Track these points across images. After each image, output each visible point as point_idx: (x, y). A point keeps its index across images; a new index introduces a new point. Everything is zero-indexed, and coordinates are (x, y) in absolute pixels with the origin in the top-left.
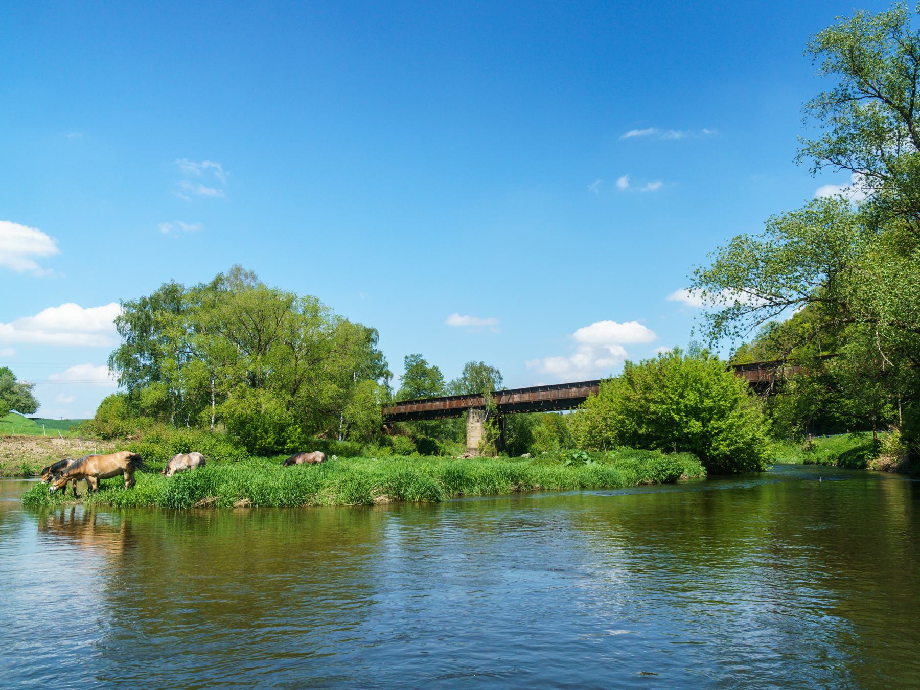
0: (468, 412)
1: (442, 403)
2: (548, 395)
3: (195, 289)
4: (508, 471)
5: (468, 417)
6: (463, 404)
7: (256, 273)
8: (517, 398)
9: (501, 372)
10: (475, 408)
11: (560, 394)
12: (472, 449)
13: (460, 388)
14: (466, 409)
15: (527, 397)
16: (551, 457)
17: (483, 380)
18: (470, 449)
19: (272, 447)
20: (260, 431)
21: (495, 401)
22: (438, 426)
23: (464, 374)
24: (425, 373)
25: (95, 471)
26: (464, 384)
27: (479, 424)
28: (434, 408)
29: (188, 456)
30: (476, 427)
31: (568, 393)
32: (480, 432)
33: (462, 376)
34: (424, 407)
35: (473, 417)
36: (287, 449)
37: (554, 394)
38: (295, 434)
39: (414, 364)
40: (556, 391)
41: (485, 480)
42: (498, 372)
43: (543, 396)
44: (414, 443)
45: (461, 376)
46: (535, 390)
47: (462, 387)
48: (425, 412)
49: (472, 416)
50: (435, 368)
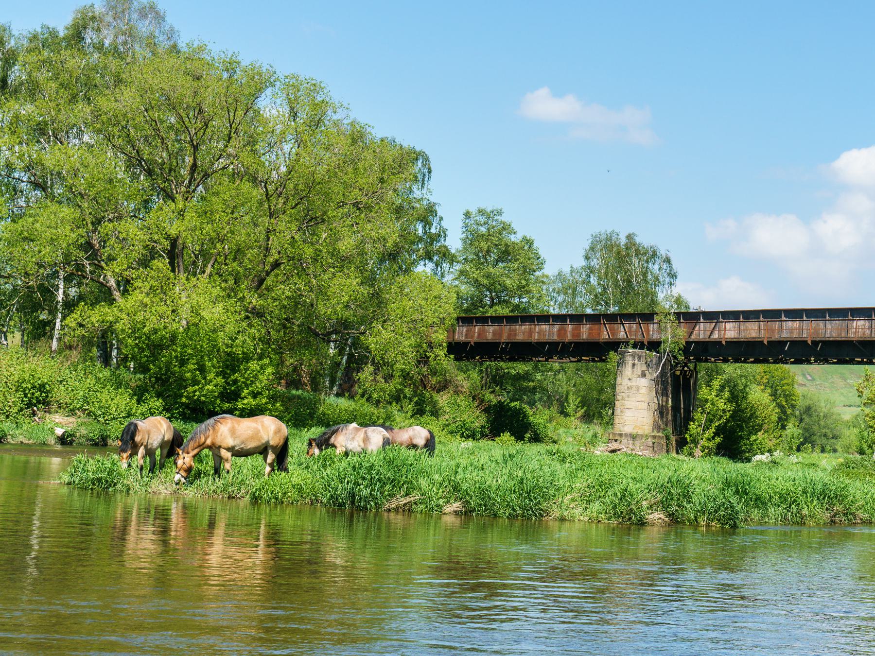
0: (623, 354)
1: (556, 328)
2: (801, 330)
3: (35, 37)
4: (819, 487)
5: (621, 363)
6: (605, 336)
7: (161, 7)
8: (730, 331)
9: (673, 261)
11: (831, 330)
12: (626, 435)
13: (575, 290)
14: (614, 345)
15: (753, 331)
16: (866, 468)
17: (631, 276)
18: (621, 435)
19: (213, 403)
20: (191, 367)
21: (682, 331)
22: (526, 377)
23: (587, 258)
24: (506, 254)
25: (230, 442)
26: (586, 282)
28: (536, 338)
29: (366, 432)
31: (848, 329)
32: (646, 398)
33: (583, 263)
34: (513, 333)
35: (634, 365)
37: (816, 330)
38: (260, 377)
39: (483, 230)
40: (821, 324)
41: (785, 500)
42: (668, 261)
43: (790, 330)
45: (581, 263)
46: (772, 315)
47: (580, 288)
49: (631, 362)
50: (529, 242)
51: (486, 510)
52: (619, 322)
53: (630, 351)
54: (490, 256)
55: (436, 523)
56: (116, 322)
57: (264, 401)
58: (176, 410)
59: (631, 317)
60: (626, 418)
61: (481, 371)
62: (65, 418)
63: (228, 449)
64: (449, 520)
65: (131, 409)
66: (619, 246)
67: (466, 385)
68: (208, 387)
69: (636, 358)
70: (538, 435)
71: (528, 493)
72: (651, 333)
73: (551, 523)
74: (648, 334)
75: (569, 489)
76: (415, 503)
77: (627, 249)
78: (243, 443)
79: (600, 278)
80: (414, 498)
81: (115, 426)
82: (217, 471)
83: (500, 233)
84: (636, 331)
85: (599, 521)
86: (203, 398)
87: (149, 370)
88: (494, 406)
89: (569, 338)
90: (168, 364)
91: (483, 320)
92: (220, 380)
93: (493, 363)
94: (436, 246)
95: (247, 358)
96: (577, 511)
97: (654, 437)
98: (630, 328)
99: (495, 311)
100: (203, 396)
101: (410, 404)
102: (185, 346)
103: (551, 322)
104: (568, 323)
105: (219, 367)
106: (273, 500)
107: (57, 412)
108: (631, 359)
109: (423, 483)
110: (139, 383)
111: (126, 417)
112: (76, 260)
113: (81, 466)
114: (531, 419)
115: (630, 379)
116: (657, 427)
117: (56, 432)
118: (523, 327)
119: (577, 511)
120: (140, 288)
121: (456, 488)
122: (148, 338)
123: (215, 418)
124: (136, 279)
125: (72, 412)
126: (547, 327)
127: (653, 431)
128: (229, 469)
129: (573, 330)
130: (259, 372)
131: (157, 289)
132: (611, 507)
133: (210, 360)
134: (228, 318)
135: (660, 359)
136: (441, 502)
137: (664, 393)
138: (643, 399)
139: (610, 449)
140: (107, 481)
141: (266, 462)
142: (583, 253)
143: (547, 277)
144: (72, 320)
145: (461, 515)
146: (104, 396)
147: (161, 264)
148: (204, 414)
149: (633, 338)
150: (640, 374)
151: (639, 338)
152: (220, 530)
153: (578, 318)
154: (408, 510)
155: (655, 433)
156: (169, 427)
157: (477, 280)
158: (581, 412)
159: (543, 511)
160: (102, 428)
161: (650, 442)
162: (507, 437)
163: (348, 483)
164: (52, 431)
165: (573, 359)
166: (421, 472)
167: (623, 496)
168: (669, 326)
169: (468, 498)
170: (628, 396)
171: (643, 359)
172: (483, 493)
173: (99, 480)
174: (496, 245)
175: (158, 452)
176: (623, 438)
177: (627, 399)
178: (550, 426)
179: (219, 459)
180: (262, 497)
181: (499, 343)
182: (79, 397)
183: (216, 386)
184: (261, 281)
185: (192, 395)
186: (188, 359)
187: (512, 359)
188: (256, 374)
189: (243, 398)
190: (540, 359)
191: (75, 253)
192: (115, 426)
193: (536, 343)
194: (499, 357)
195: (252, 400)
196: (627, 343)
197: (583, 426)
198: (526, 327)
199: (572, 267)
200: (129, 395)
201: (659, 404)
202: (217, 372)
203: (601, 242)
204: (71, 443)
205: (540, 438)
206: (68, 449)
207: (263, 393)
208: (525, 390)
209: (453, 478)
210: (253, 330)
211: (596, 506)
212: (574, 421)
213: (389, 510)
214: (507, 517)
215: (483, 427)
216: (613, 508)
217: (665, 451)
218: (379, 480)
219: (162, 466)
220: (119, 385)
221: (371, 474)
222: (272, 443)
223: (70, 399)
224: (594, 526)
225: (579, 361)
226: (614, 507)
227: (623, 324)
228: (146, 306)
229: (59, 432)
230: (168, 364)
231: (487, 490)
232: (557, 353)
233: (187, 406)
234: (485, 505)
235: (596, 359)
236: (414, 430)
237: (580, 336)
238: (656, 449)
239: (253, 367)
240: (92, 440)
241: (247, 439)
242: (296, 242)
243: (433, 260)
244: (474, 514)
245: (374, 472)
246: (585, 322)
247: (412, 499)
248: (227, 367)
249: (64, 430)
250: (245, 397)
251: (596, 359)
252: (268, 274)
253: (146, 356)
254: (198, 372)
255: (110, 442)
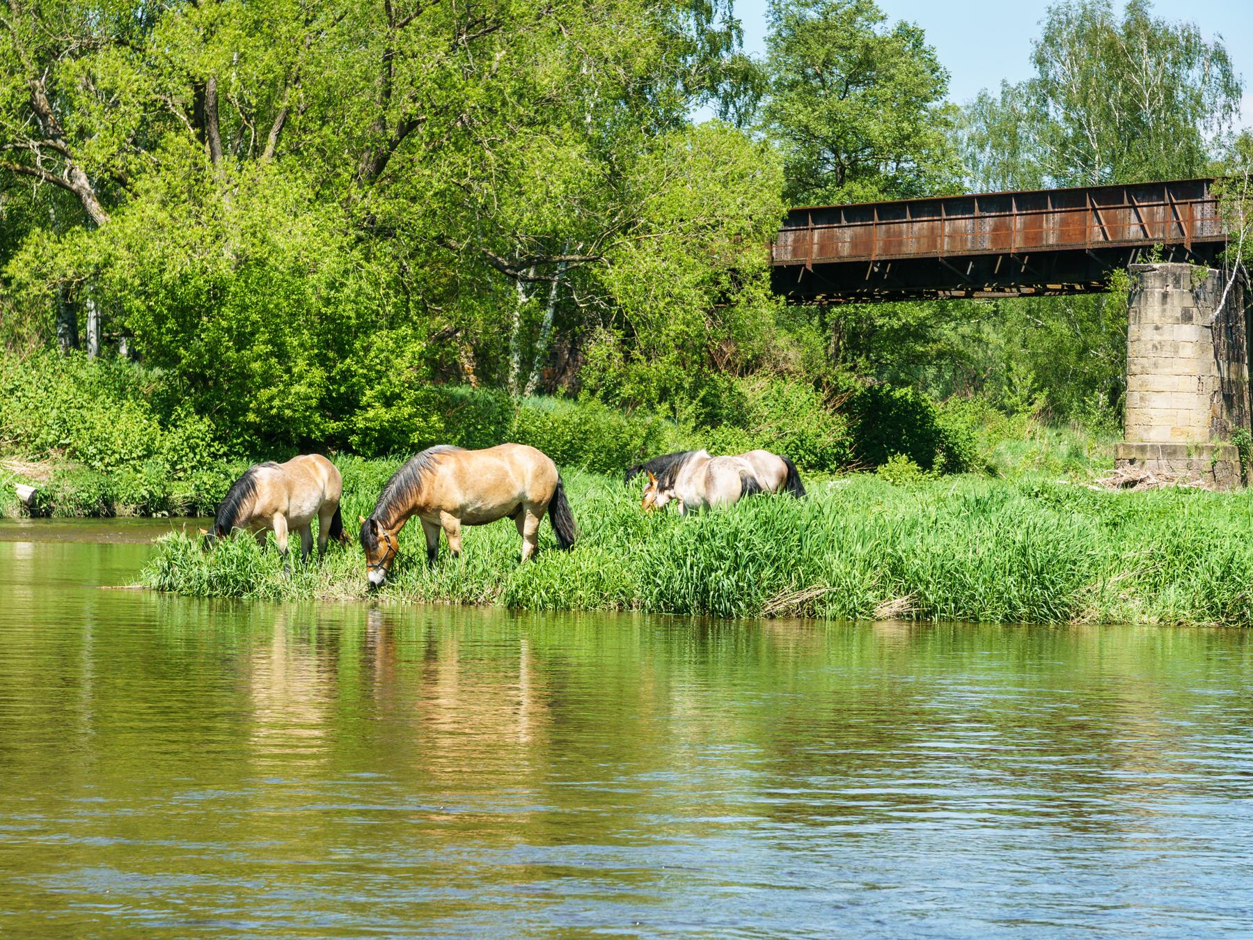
0: (1140, 274)
1: (988, 224)
5: (1136, 294)
10: (1175, 252)
13: (1014, 137)
14: (1118, 255)
18: (1142, 449)
19: (307, 421)
22: (918, 332)
23: (1041, 61)
25: (457, 498)
27: (1189, 332)
28: (945, 248)
30: (1176, 348)
32: (1195, 368)
33: (1034, 73)
34: (894, 241)
35: (1165, 296)
36: (366, 432)
38: (397, 362)
42: (1220, 57)
44: (840, 411)
48: (894, 262)
49: (1158, 292)
51: (957, 609)
52: (1126, 203)
53: (1156, 266)
54: (831, 73)
55: (862, 639)
56: (107, 264)
57: (407, 411)
58: (238, 438)
59: (1152, 191)
60: (1152, 412)
61: (824, 325)
62: (31, 464)
63: (454, 512)
64: (889, 630)
65: (153, 440)
66: (1109, 31)
67: (795, 357)
68: (296, 388)
69: (1170, 280)
70: (957, 456)
71: (1039, 574)
72: (1199, 223)
73: (1086, 630)
74: (1192, 227)
75: (1115, 564)
76: (821, 602)
77: (1129, 35)
78: (479, 498)
79: (1069, 106)
80: (818, 592)
81: (125, 475)
82: (432, 554)
83: (852, 21)
84: (1165, 222)
85: (1180, 624)
86: (288, 412)
87: (177, 359)
88: (859, 398)
89: (1017, 244)
90: (213, 349)
91: (829, 215)
92: (318, 374)
93: (851, 309)
94: (726, 58)
95: (367, 326)
96: (1135, 605)
97: (1213, 450)
98: (1151, 215)
99: (849, 194)
100: (289, 406)
101: (691, 403)
102: (245, 308)
103: (977, 213)
104: (1015, 211)
105: (312, 347)
106: (550, 606)
107: (13, 453)
108: (1158, 284)
109: (839, 567)
110: (161, 387)
111: (144, 456)
112: (14, 141)
113: (179, 555)
114: (939, 423)
115: (1157, 328)
116: (1220, 429)
117: (18, 492)
118: (917, 226)
119: (1135, 605)
120: (147, 191)
121: (897, 569)
122: (171, 293)
123: (426, 452)
124: (138, 173)
125: (41, 452)
126: (969, 223)
127: (1211, 437)
128: (458, 549)
129: (1026, 226)
130: (393, 352)
131: (182, 193)
132: (1202, 596)
133: (297, 331)
134: (326, 245)
135: (1222, 281)
136: (870, 597)
137: (1234, 356)
138: (1187, 370)
139: (1122, 480)
140: (237, 582)
141: (522, 535)
142: (1032, 49)
143: (956, 109)
144: (21, 264)
145: (910, 622)
146: (98, 417)
147: (181, 140)
148: (288, 443)
149: (1164, 234)
150: (1179, 315)
151: (1172, 236)
152: (448, 669)
153: (1033, 201)
154: (808, 614)
155: (1217, 442)
156: (332, 475)
157: (806, 127)
158: (1041, 400)
159: (1070, 607)
160: (103, 480)
161: (1206, 460)
162: (900, 464)
163: (692, 568)
164: (10, 489)
165: (1025, 290)
166: (832, 542)
167: (1227, 571)
168: (1238, 205)
169: (921, 588)
170: (1156, 365)
171: (1185, 283)
172: (951, 577)
173: (223, 580)
174: (842, 47)
175: (315, 524)
176: (1148, 455)
177: (1153, 371)
178: (980, 435)
179: (433, 527)
180: (528, 600)
181: (867, 264)
182: (50, 422)
183: (310, 385)
184: (381, 163)
185: (267, 405)
186: (253, 334)
187: (894, 297)
188: (387, 358)
189: (364, 408)
190: (955, 293)
191: (11, 127)
192: (125, 475)
193: (947, 259)
194: (867, 295)
195: (384, 410)
196: (1146, 250)
197: (1048, 431)
198: (921, 226)
199: (1004, 84)
200: (145, 413)
201: (1222, 379)
202: (310, 358)
203: (1069, 22)
204: (48, 514)
205: (959, 463)
206: (41, 523)
207: (404, 395)
208: (920, 359)
209: (890, 550)
210: (373, 267)
211: (1171, 594)
212: (1026, 423)
213: (772, 617)
214: (1002, 622)
215: (840, 444)
216: (1207, 596)
217: (1237, 479)
218: (753, 559)
219: (323, 550)
220: (122, 393)
221: (734, 548)
222: (530, 496)
223: (34, 425)
224: (1170, 632)
225: (1038, 293)
226: (1209, 596)
227: (1135, 208)
228: (161, 227)
229: (25, 492)
230: (213, 349)
231: (957, 571)
232: (992, 278)
233: (256, 428)
234: (955, 601)
235: (1078, 287)
236: (753, 458)
237: (1041, 239)
238: (1219, 476)
239: (379, 343)
240: (86, 505)
241: (487, 491)
242: (450, 75)
243: (716, 91)
244: (935, 619)
245: (740, 545)
246: (1050, 209)
247: (814, 593)
248: (327, 346)
249: (33, 489)
250: (369, 405)
251: (1078, 287)
252: (393, 145)
253: (169, 331)
254: (273, 360)
255: (119, 508)
